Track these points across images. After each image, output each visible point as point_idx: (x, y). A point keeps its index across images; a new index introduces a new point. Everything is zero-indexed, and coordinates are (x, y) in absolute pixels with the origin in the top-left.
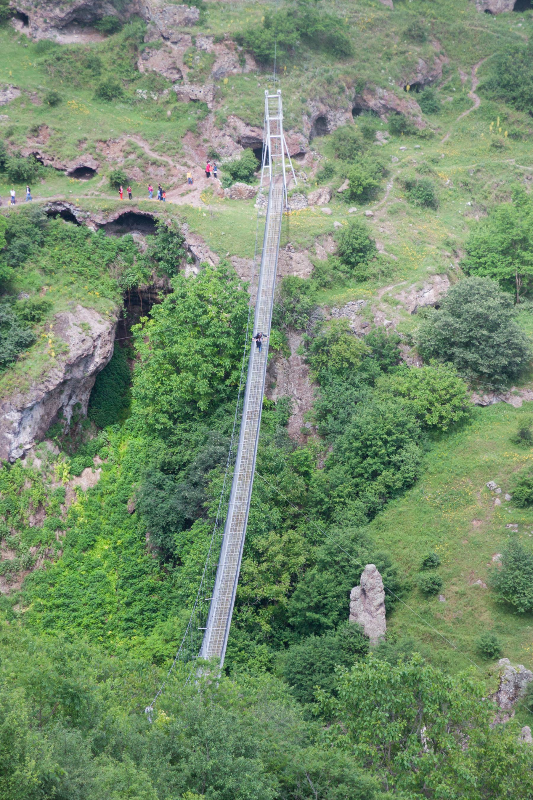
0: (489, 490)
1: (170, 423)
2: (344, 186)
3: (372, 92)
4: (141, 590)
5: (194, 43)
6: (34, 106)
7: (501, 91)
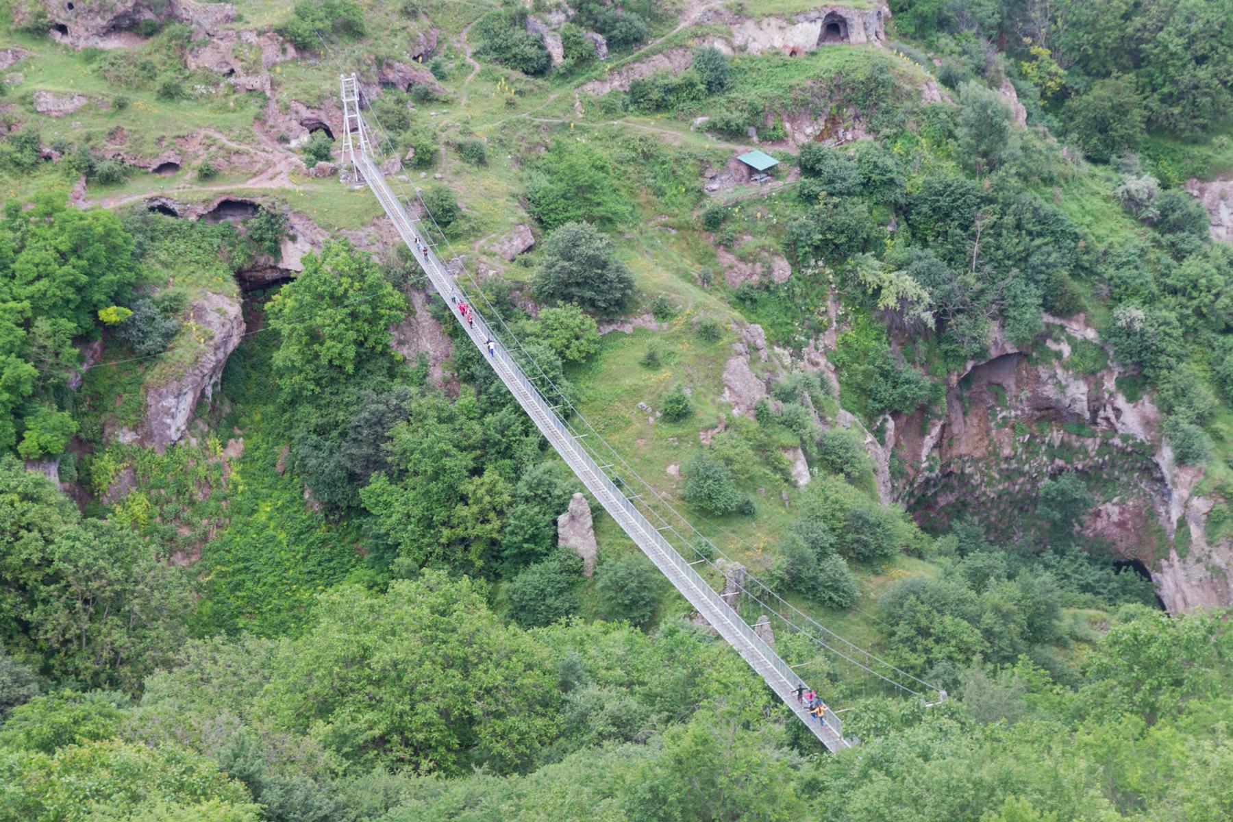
0: (642, 410)
1: (318, 390)
2: (410, 154)
3: (390, 66)
4: (313, 543)
5: (239, 37)
6: (103, 110)
7: (494, 55)
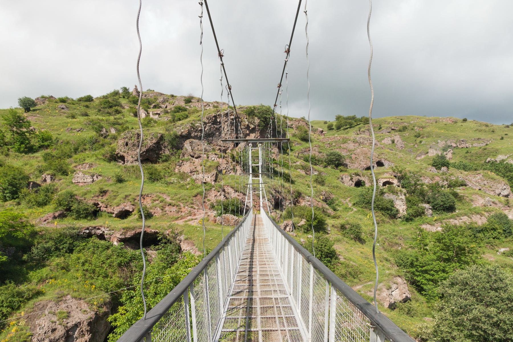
2: (303, 222)
